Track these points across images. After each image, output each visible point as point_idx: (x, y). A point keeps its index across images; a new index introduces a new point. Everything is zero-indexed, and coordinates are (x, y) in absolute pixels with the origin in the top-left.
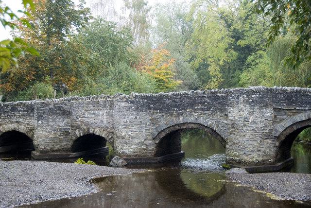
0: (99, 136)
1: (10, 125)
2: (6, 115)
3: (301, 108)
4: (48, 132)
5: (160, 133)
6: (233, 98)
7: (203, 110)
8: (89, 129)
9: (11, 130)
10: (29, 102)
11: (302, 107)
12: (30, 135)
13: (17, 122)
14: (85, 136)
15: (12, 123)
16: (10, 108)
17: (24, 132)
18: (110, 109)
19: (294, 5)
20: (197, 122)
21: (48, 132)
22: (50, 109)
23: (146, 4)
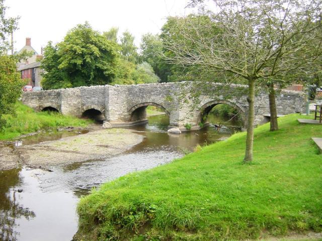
13: (51, 102)
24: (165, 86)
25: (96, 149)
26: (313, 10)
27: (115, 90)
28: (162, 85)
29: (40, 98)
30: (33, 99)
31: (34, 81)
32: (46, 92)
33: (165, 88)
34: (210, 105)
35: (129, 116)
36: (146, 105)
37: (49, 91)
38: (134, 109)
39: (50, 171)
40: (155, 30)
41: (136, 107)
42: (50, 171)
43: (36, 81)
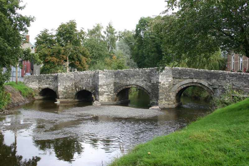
0: (121, 91)
1: (46, 85)
2: (44, 80)
3: (185, 78)
4: (63, 89)
5: (179, 87)
6: (154, 72)
7: (139, 78)
8: (83, 88)
9: (46, 88)
10: (54, 74)
11: (186, 77)
12: (55, 90)
13: (49, 84)
14: (81, 91)
15: (46, 84)
16: (46, 77)
17: (52, 89)
18: (94, 78)
19: (220, 54)
20: (199, 82)
21: (63, 89)
22: (64, 77)
23: (28, 26)
24: (147, 71)
25: (178, 89)
26: (160, 72)
27: (104, 74)
28: (143, 70)
29: (40, 81)
30: (33, 81)
31: (32, 69)
32: (45, 76)
33: (146, 73)
34: (185, 86)
35: (115, 96)
36: (129, 87)
37: (47, 75)
38: (120, 90)
39: (22, 132)
40: (132, 27)
41: (121, 89)
42: (22, 132)
43: (34, 69)
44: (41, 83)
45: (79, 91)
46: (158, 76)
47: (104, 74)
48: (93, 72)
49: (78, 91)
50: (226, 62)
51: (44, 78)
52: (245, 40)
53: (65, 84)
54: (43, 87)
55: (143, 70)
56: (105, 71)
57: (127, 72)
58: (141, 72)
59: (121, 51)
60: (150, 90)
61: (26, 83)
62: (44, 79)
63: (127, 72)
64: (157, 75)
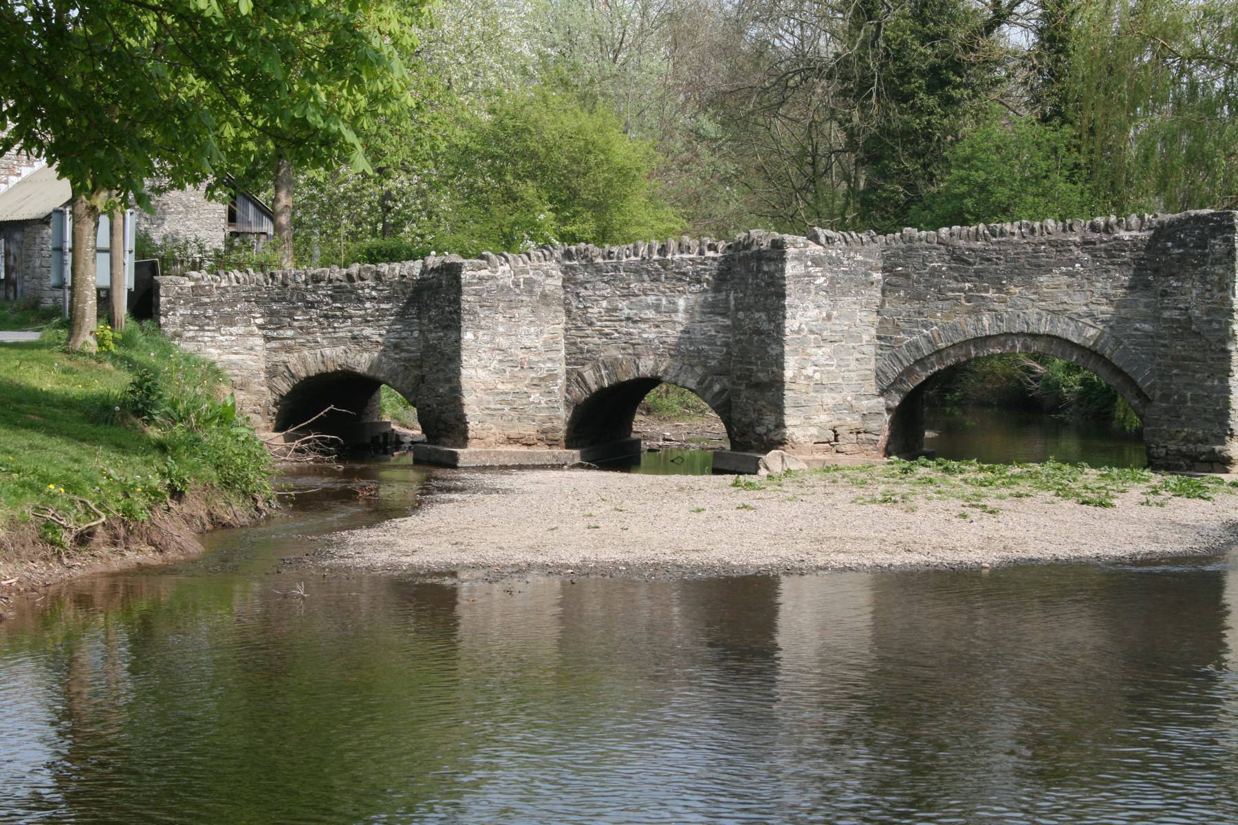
9: (331, 368)
16: (324, 290)
29: (275, 320)
30: (229, 320)
32: (316, 279)
44: (290, 333)
45: (602, 390)
46: (1219, 270)
47: (816, 262)
48: (712, 247)
49: (594, 388)
50: (428, 479)
51: (309, 298)
52: (247, 35)
53: (507, 335)
54: (304, 361)
55: (1094, 228)
56: (823, 240)
57: (979, 244)
58: (1086, 242)
59: (144, 19)
60: (948, 397)
61: (177, 335)
62: (310, 305)
63: (979, 244)
64: (1217, 261)
